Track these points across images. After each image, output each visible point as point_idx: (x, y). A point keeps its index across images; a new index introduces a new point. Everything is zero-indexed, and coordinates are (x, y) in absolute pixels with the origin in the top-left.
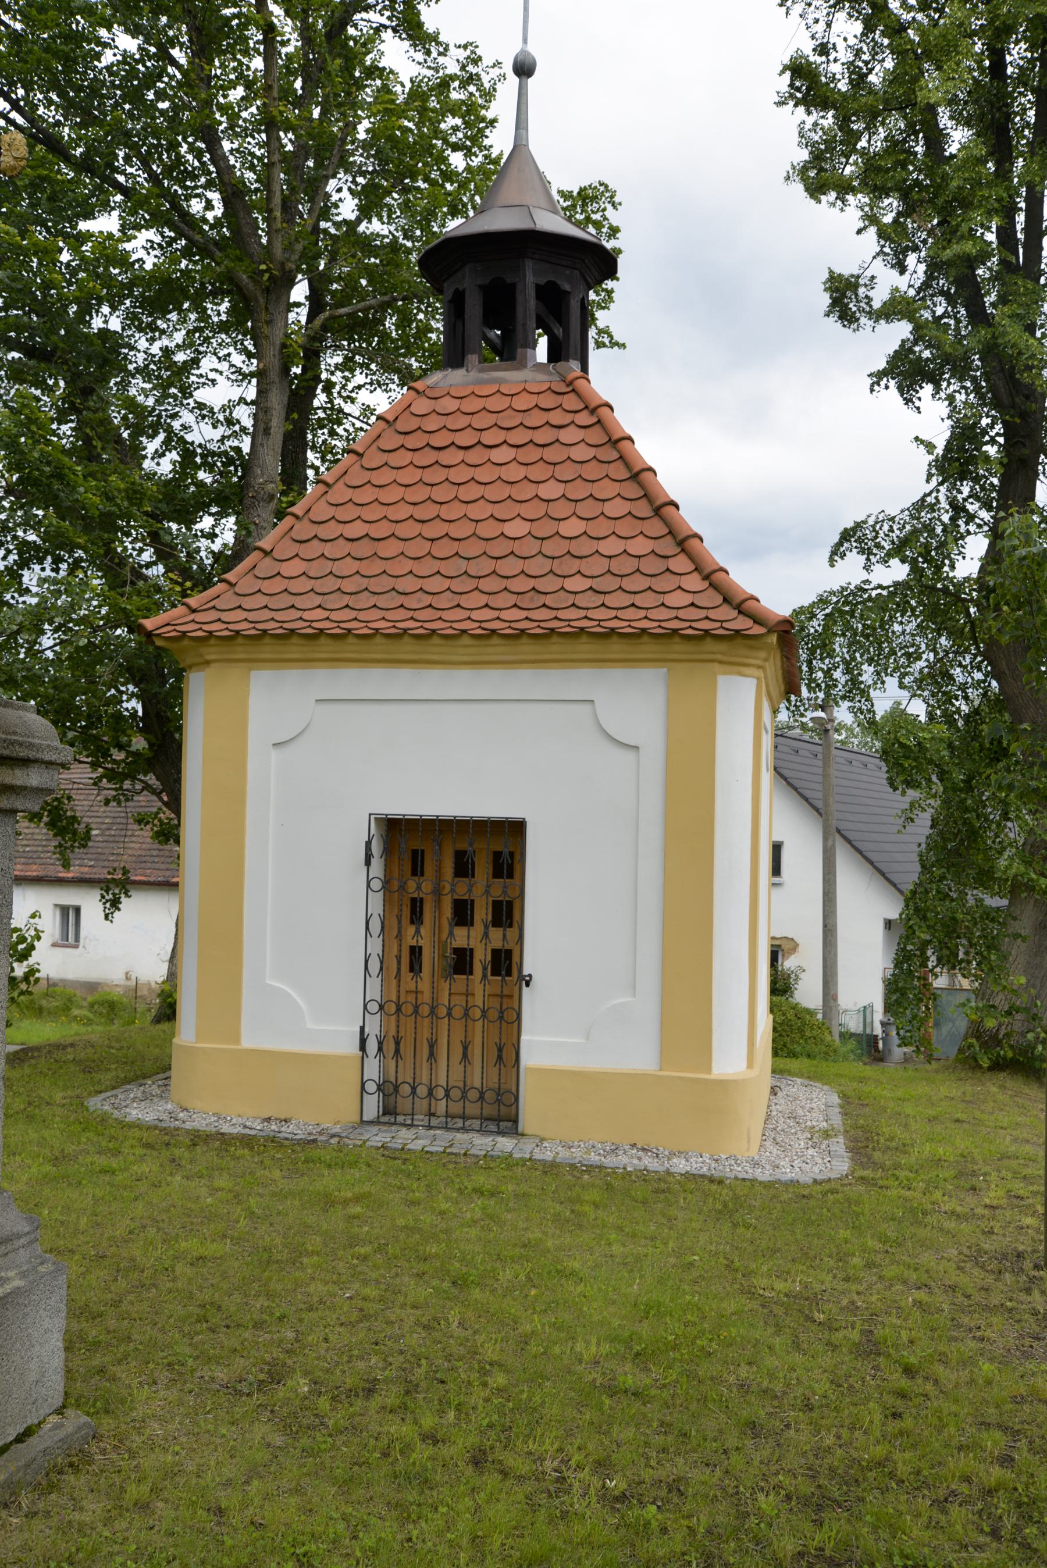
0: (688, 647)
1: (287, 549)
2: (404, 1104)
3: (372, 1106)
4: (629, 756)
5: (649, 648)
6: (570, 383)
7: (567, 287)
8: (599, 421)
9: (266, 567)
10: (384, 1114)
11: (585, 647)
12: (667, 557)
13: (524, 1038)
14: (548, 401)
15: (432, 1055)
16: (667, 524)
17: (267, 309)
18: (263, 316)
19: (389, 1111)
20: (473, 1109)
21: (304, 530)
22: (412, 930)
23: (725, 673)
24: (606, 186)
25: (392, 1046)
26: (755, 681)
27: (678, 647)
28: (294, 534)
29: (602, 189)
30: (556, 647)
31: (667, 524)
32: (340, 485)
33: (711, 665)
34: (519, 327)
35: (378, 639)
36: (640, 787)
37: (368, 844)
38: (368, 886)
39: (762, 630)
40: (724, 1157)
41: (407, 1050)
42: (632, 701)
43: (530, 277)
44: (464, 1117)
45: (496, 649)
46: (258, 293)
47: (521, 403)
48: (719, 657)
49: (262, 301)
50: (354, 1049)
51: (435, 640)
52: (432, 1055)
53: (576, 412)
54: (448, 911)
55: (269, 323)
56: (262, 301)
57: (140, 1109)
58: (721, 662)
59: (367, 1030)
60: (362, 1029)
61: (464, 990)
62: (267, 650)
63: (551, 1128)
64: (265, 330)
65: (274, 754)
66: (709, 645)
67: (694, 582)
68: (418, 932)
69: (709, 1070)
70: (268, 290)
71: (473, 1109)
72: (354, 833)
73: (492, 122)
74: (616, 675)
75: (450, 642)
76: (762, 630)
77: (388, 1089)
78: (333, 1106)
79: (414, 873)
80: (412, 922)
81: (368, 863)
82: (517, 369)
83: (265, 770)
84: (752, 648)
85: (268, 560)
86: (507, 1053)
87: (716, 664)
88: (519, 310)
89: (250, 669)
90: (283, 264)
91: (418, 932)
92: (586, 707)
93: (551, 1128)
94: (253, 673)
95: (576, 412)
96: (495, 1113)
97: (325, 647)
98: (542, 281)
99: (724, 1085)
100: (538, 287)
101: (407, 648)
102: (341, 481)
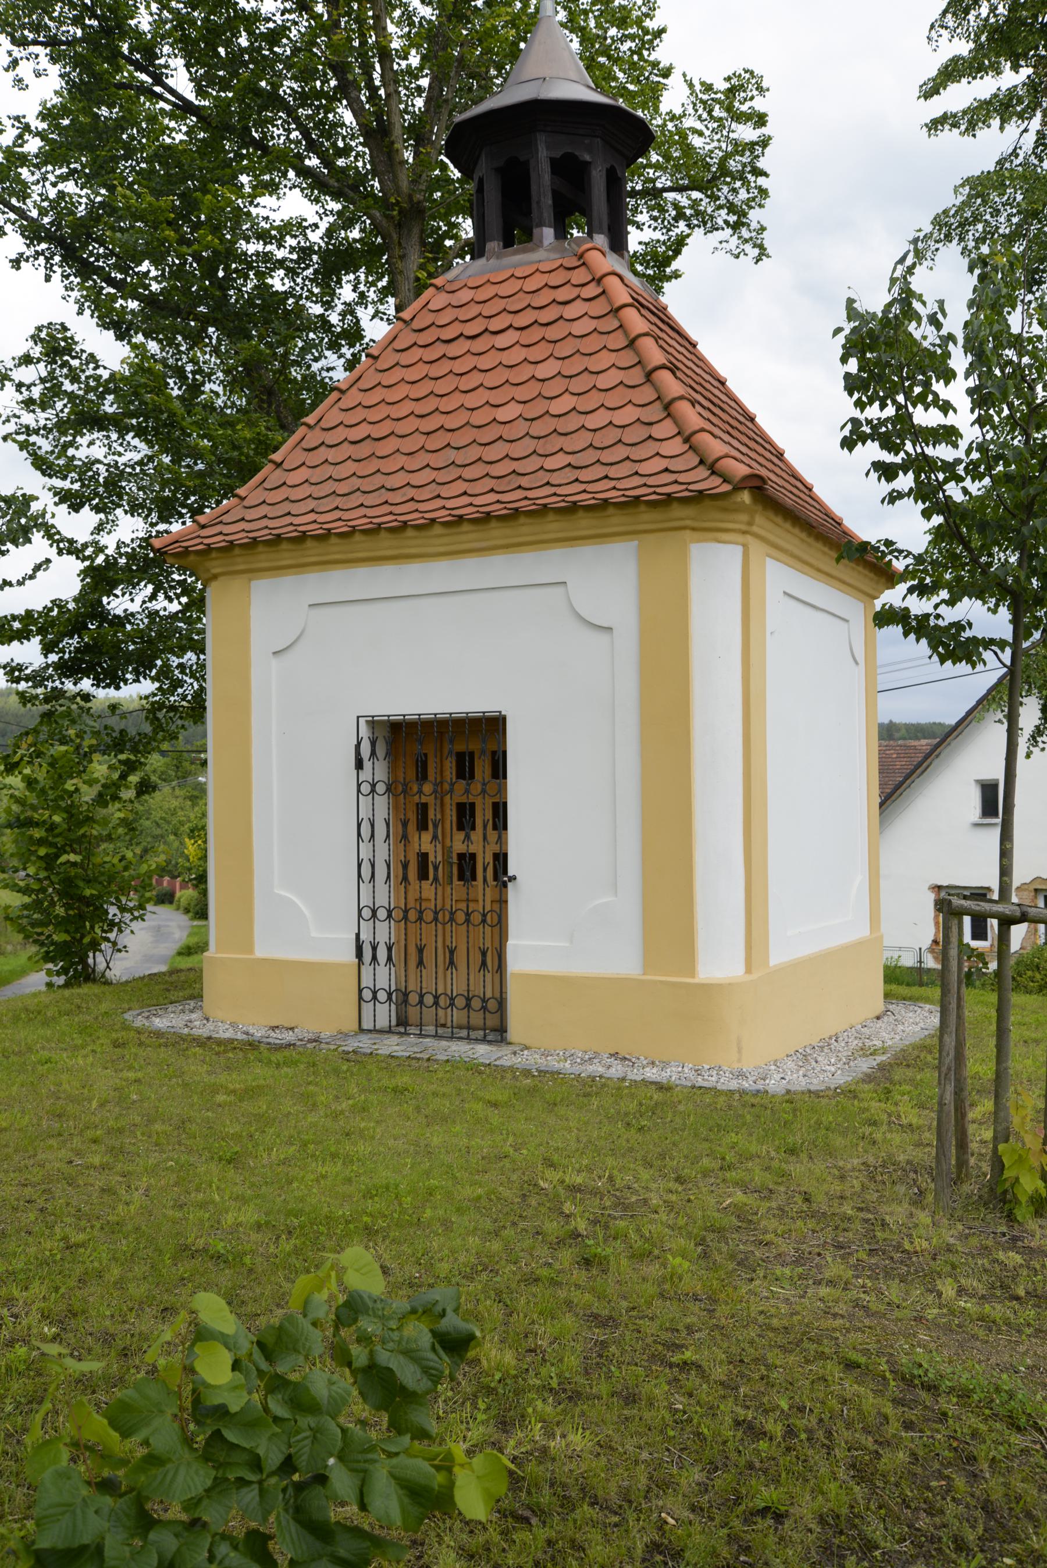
0: (655, 515)
1: (299, 457)
2: (413, 1013)
3: (384, 1014)
4: (603, 638)
5: (616, 521)
6: (581, 257)
7: (587, 158)
8: (604, 292)
9: (276, 477)
10: (397, 1025)
11: (553, 526)
12: (651, 424)
13: (511, 943)
14: (555, 279)
15: (421, 963)
16: (656, 389)
17: (400, 244)
18: (397, 252)
19: (403, 1021)
20: (477, 1019)
21: (314, 438)
22: (460, 836)
23: (699, 541)
24: (752, 73)
25: (411, 955)
26: (740, 548)
27: (647, 517)
28: (304, 444)
29: (747, 76)
30: (525, 529)
31: (656, 389)
32: (354, 390)
33: (683, 532)
34: (534, 206)
35: (358, 537)
36: (611, 669)
37: (358, 747)
38: (359, 791)
39: (726, 488)
40: (707, 1067)
41: (428, 956)
42: (602, 578)
43: (542, 155)
44: (469, 1028)
45: (468, 535)
46: (391, 229)
47: (531, 285)
48: (688, 523)
49: (395, 236)
50: (351, 957)
51: (410, 532)
52: (421, 963)
53: (583, 285)
54: (451, 815)
55: (402, 257)
56: (395, 236)
57: (166, 1021)
58: (693, 529)
59: (363, 937)
60: (358, 935)
61: (465, 897)
62: (263, 558)
63: (540, 1037)
64: (400, 265)
65: (274, 662)
66: (678, 511)
67: (676, 446)
68: (467, 837)
69: (692, 971)
70: (399, 226)
71: (477, 1019)
72: (339, 740)
73: (660, 33)
74: (588, 552)
75: (424, 533)
76: (726, 488)
77: (401, 998)
78: (329, 1015)
79: (460, 775)
80: (460, 827)
81: (359, 765)
82: (532, 250)
83: (267, 677)
84: (725, 510)
85: (278, 471)
86: (494, 959)
87: (688, 532)
88: (534, 188)
89: (250, 580)
90: (410, 196)
91: (467, 837)
92: (560, 589)
93: (540, 1037)
94: (254, 583)
95: (583, 285)
96: (464, 1022)
97: (312, 551)
98: (558, 154)
99: (708, 989)
100: (553, 162)
101: (386, 544)
102: (355, 387)
